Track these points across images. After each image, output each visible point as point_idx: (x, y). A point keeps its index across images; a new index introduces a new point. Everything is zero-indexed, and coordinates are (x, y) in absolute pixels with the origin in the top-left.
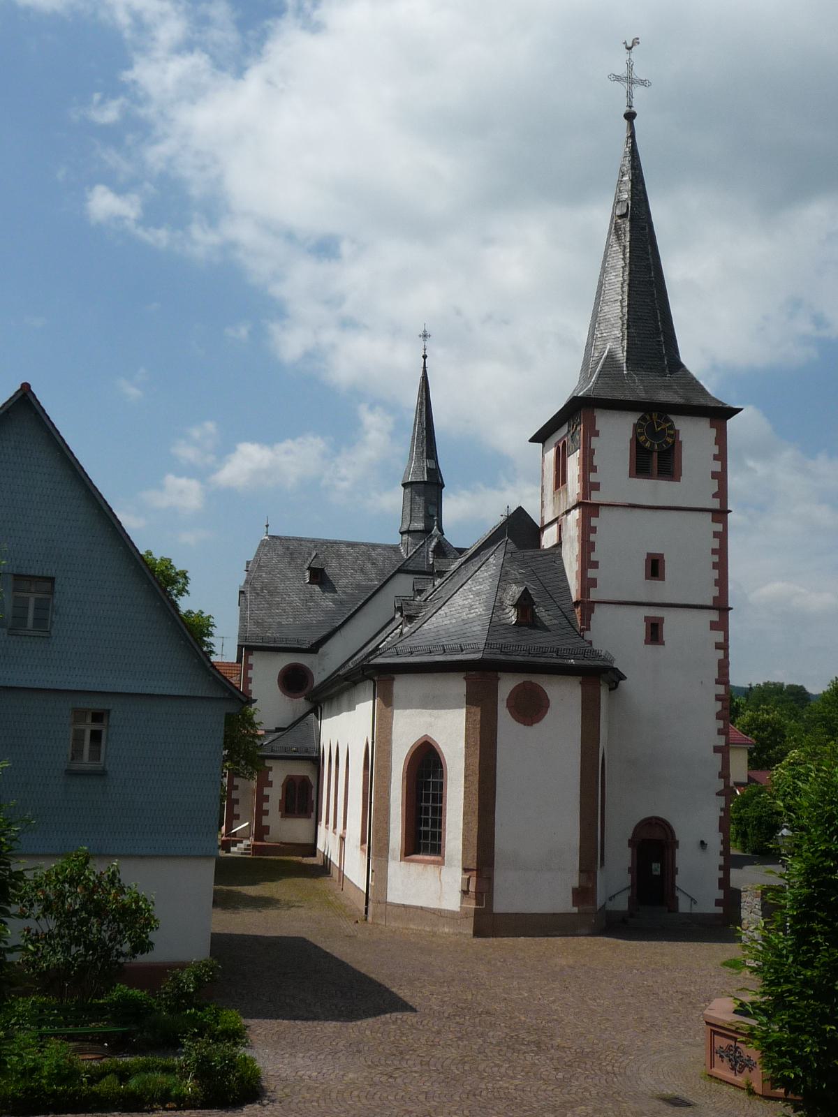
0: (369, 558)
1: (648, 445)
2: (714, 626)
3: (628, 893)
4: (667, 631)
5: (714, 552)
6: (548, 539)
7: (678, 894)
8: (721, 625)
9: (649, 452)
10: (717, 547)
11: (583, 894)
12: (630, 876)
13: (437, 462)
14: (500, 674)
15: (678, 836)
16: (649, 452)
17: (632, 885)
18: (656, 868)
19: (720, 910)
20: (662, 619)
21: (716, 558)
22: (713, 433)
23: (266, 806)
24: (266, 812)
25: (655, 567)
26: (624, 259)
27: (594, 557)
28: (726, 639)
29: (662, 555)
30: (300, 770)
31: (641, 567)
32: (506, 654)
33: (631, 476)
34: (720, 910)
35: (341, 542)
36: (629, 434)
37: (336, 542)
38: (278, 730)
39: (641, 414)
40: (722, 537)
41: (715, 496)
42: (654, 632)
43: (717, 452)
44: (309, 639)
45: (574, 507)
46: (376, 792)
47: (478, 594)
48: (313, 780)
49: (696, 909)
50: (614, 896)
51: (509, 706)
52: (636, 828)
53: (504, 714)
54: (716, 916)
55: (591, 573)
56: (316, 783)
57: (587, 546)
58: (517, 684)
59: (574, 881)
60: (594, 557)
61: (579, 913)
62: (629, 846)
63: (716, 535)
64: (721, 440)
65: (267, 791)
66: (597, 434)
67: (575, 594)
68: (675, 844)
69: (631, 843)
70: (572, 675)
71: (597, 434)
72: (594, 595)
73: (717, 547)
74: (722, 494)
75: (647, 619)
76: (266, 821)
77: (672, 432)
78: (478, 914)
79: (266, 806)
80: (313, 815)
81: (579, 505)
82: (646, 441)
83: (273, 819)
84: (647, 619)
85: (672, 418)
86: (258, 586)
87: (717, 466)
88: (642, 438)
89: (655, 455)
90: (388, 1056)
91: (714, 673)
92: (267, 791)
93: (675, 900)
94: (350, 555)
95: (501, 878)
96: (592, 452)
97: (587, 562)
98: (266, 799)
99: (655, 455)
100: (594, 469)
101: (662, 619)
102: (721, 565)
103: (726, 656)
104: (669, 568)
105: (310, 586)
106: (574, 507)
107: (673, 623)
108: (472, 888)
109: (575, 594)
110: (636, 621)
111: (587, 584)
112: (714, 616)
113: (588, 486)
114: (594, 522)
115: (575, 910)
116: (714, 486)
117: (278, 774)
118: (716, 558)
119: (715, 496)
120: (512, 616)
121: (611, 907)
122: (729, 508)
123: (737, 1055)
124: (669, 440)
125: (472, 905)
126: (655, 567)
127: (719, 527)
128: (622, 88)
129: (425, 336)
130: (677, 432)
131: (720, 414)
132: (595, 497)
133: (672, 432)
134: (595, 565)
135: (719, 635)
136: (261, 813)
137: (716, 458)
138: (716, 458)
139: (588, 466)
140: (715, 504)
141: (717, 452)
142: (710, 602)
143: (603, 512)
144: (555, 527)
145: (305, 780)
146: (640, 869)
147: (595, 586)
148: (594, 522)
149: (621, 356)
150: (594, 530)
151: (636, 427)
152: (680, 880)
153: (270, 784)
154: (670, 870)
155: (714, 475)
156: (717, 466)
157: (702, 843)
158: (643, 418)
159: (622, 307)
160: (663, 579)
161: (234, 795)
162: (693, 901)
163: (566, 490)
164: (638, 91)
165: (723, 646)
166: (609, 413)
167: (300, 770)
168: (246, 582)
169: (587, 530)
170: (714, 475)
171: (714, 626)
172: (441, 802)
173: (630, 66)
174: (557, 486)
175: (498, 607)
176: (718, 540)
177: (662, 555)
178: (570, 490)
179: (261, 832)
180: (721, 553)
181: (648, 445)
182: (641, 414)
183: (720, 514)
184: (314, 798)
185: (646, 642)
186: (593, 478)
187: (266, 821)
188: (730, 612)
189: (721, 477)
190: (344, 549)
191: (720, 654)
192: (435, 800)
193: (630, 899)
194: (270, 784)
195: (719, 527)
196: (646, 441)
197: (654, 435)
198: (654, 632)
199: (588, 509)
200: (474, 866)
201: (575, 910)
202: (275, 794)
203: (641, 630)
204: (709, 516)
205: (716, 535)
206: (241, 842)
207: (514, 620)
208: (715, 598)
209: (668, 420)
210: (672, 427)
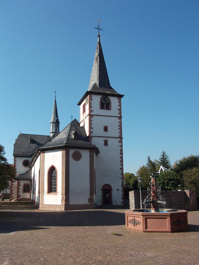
0: (43, 138)
1: (104, 102)
2: (119, 142)
3: (101, 201)
4: (109, 143)
5: (119, 126)
6: (82, 125)
7: (113, 201)
8: (121, 142)
9: (104, 104)
10: (120, 125)
11: (91, 200)
12: (101, 197)
13: (58, 118)
14: (70, 149)
15: (112, 188)
16: (104, 104)
17: (102, 199)
18: (107, 195)
19: (122, 204)
20: (108, 140)
21: (119, 127)
22: (118, 100)
23: (19, 190)
24: (19, 192)
25: (106, 129)
26: (98, 64)
27: (92, 126)
28: (122, 145)
29: (107, 126)
30: (27, 182)
31: (102, 129)
32: (71, 144)
33: (100, 109)
34: (122, 204)
35: (37, 135)
36: (99, 100)
37: (36, 135)
38: (22, 174)
39: (102, 96)
40: (121, 122)
41: (119, 114)
42: (106, 143)
43: (119, 104)
44: (30, 154)
45: (87, 116)
46: (41, 179)
47: (65, 133)
48: (30, 184)
49: (117, 204)
50: (98, 202)
51: (72, 156)
52: (103, 187)
53: (71, 159)
54: (122, 205)
55: (91, 130)
56: (31, 184)
57: (90, 124)
58: (73, 152)
59: (89, 197)
60: (92, 126)
61: (90, 204)
62: (101, 190)
63: (119, 122)
64: (120, 102)
65: (19, 187)
66: (92, 100)
67: (88, 135)
68: (112, 190)
69: (102, 190)
70: (87, 149)
71: (92, 100)
72: (92, 135)
73: (120, 125)
74: (120, 113)
75: (104, 140)
76: (19, 194)
77: (109, 100)
78: (65, 205)
79: (19, 190)
80: (30, 192)
81: (89, 115)
82: (103, 102)
83: (21, 193)
84: (104, 140)
85: (109, 97)
86: (18, 144)
87: (119, 108)
88: (102, 101)
89: (105, 105)
90: (79, 262)
91: (120, 152)
92: (19, 187)
93: (112, 202)
94: (39, 138)
95: (71, 196)
96: (91, 104)
97: (90, 128)
98: (19, 189)
99: (105, 105)
100: (92, 107)
101: (108, 140)
102: (121, 129)
103: (122, 148)
104: (109, 129)
105: (30, 144)
106: (87, 116)
107: (110, 141)
108: (64, 199)
109: (88, 135)
110: (102, 141)
111: (91, 132)
112: (119, 140)
113: (91, 111)
114: (92, 119)
115: (89, 203)
116: (118, 112)
117: (22, 183)
118: (119, 127)
119: (119, 114)
120: (73, 137)
121: (97, 204)
122: (122, 116)
123: (135, 221)
124: (109, 102)
125: (64, 203)
126: (106, 129)
127: (120, 120)
128: (97, 30)
129: (55, 92)
130: (110, 100)
131: (120, 96)
132: (92, 113)
133: (109, 100)
134: (92, 128)
135: (120, 144)
136: (18, 192)
137: (119, 106)
138: (119, 106)
139: (90, 107)
140: (119, 115)
141: (119, 104)
142: (118, 137)
143: (94, 117)
144: (83, 121)
145: (28, 184)
146: (104, 196)
147: (92, 133)
148: (92, 119)
149: (98, 84)
150: (92, 121)
151: (101, 98)
152: (113, 198)
153: (20, 185)
154: (111, 196)
155: (118, 109)
156: (119, 108)
157: (118, 189)
158: (102, 97)
159: (98, 74)
160: (108, 131)
161: (12, 189)
162: (116, 202)
163: (85, 113)
164: (100, 31)
165: (121, 146)
166: (95, 95)
167: (27, 182)
168: (15, 143)
169: (90, 121)
170: (118, 109)
171: (119, 142)
172: (56, 180)
173: (99, 26)
174: (83, 113)
175: (69, 135)
176: (120, 123)
177: (107, 126)
178: (86, 114)
179: (18, 196)
180: (120, 126)
181: (104, 102)
182: (102, 96)
183: (120, 118)
184: (30, 188)
185: (104, 145)
186: (91, 109)
187: (19, 194)
188: (123, 139)
189: (120, 110)
190: (38, 136)
191: (121, 148)
192: (55, 180)
193: (102, 202)
194: (20, 185)
195: (120, 120)
196: (103, 102)
197: (105, 100)
198: (106, 143)
199: (91, 116)
200: (64, 194)
201: (89, 203)
202: (21, 188)
203: (103, 143)
204: (118, 118)
205: (119, 122)
206: (14, 199)
207: (73, 137)
208: (119, 136)
209: (108, 97)
210: (109, 99)
